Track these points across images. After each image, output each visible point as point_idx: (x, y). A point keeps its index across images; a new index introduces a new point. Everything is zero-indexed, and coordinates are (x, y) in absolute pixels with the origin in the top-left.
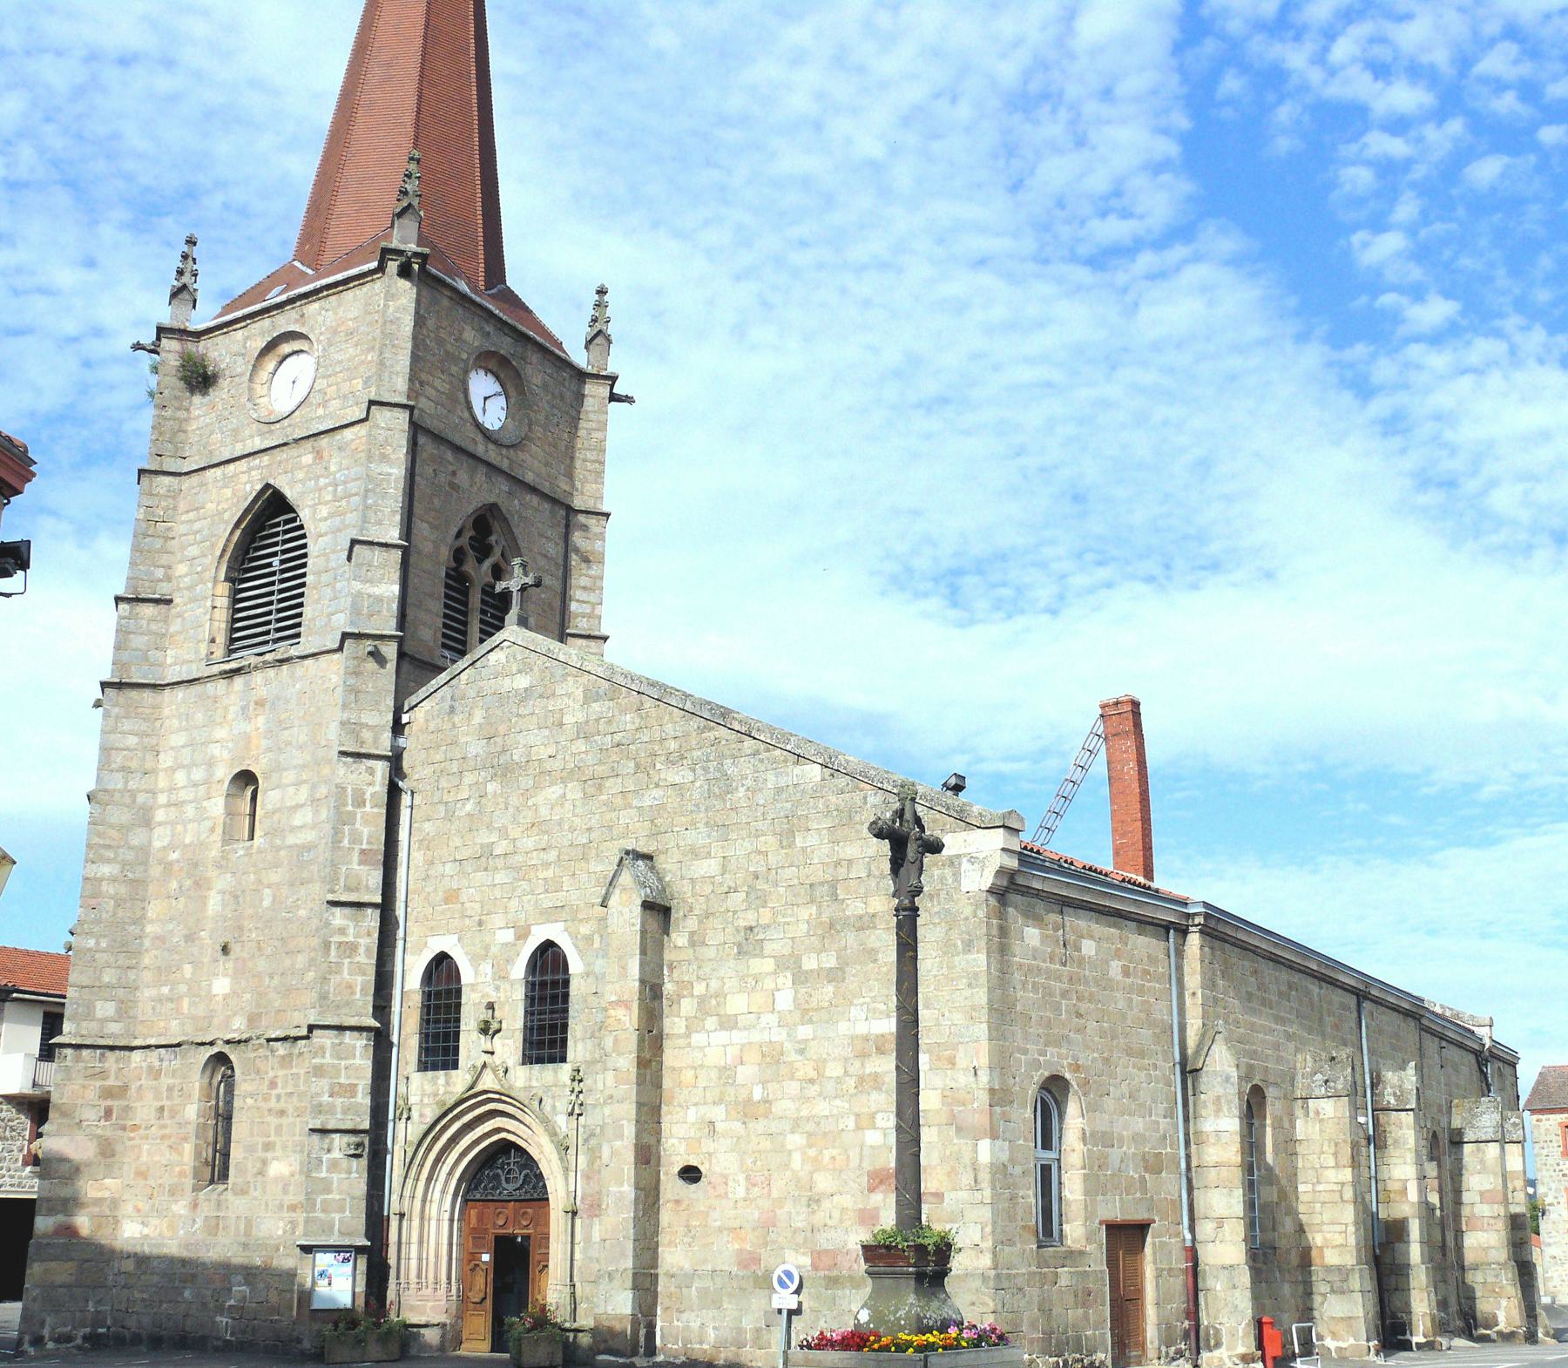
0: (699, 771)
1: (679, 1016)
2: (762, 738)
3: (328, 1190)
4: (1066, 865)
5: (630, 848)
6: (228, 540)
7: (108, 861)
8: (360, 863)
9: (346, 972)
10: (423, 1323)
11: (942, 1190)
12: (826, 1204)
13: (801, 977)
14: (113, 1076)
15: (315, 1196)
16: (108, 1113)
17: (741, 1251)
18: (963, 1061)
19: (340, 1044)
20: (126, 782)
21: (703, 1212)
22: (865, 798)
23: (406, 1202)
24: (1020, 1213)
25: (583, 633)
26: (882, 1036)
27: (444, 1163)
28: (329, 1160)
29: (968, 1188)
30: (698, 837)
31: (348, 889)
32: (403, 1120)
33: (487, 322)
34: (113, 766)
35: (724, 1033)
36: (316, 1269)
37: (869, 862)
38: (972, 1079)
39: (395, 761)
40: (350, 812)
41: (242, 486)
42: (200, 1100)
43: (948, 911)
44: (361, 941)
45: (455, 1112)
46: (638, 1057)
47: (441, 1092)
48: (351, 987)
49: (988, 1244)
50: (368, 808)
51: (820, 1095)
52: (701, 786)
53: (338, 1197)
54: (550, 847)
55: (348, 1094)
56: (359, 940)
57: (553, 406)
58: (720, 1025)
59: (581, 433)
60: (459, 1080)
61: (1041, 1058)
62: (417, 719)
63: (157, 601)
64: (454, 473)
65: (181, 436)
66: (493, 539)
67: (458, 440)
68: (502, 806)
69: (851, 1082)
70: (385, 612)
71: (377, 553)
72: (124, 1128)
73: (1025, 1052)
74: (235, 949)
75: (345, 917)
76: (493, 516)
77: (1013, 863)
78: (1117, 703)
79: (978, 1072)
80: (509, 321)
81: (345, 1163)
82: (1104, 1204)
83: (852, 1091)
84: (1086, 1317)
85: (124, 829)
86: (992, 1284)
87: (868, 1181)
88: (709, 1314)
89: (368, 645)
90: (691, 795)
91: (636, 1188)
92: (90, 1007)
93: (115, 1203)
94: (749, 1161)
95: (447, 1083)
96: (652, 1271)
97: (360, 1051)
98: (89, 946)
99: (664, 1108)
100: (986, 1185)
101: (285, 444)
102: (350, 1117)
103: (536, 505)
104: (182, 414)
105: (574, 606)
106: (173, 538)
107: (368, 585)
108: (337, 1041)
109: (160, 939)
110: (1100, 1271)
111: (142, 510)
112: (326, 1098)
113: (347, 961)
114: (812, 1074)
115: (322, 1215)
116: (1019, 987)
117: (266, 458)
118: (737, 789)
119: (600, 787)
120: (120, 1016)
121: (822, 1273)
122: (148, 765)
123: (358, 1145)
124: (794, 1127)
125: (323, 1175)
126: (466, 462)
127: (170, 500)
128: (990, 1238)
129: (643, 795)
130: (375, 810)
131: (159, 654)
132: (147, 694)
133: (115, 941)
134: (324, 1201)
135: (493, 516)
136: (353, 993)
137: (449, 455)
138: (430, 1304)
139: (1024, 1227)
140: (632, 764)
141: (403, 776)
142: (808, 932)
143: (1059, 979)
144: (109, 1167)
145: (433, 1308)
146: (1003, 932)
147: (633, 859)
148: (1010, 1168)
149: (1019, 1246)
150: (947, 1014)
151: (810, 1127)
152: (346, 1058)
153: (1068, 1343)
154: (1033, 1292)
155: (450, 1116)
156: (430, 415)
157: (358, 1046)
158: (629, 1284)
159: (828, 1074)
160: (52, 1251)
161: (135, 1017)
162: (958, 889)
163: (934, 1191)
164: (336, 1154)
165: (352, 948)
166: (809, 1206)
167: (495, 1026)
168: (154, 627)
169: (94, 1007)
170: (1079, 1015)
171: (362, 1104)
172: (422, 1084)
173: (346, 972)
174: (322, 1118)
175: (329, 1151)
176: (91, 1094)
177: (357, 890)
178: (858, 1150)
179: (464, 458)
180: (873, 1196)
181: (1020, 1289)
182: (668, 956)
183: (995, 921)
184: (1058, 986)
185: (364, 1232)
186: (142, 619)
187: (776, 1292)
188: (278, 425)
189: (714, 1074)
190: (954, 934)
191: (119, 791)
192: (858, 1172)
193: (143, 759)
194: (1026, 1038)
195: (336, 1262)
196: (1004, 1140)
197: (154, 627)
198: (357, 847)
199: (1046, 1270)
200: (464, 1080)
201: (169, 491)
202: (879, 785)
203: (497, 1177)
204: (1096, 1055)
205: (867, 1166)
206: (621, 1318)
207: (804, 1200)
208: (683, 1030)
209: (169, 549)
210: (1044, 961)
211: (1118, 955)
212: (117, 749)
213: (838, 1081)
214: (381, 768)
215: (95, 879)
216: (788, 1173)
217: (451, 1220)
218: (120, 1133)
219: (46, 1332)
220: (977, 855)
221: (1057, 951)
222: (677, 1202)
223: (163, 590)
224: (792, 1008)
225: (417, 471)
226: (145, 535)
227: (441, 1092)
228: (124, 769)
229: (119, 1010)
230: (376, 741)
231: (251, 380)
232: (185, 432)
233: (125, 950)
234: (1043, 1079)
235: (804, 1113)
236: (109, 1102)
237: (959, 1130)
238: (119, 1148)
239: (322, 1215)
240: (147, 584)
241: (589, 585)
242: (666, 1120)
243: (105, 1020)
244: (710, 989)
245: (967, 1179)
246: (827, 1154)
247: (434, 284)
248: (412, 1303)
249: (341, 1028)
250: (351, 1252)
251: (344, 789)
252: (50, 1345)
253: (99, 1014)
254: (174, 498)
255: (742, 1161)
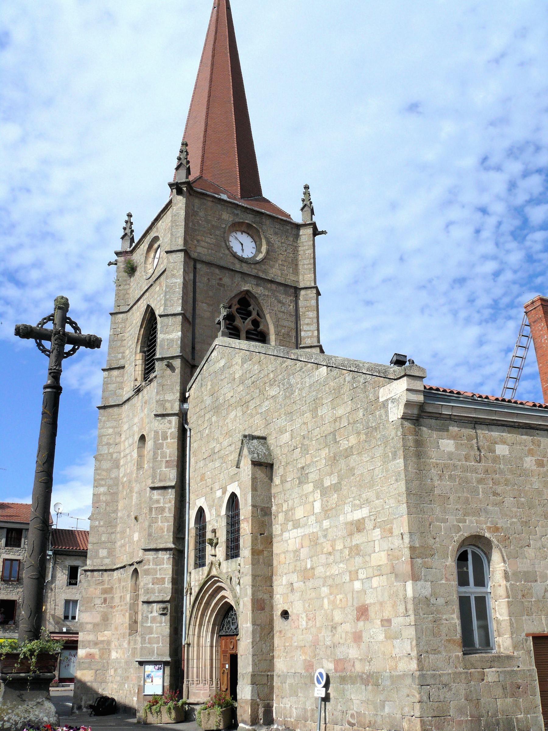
0: (281, 386)
1: (278, 524)
2: (302, 360)
3: (151, 633)
4: (479, 399)
5: (247, 434)
6: (139, 334)
7: (103, 486)
8: (166, 467)
9: (160, 522)
10: (196, 702)
11: (390, 617)
12: (339, 629)
13: (325, 492)
14: (106, 583)
15: (145, 636)
16: (105, 600)
17: (305, 660)
18: (396, 532)
19: (157, 558)
20: (109, 450)
21: (290, 637)
22: (345, 379)
23: (191, 637)
24: (444, 630)
25: (308, 345)
26: (359, 520)
28: (151, 617)
29: (403, 615)
30: (281, 422)
31: (161, 481)
32: (188, 595)
33: (236, 209)
34: (104, 443)
35: (295, 530)
36: (146, 673)
37: (348, 416)
38: (401, 542)
39: (183, 416)
40: (160, 443)
41: (141, 308)
42: (131, 592)
43: (384, 436)
44: (167, 505)
46: (252, 549)
48: (162, 529)
49: (414, 654)
50: (169, 440)
51: (334, 562)
52: (282, 394)
53: (156, 636)
54: (233, 443)
55: (161, 583)
56: (165, 505)
57: (282, 243)
58: (293, 526)
59: (301, 253)
61: (461, 525)
62: (191, 394)
63: (119, 368)
64: (221, 279)
65: (127, 296)
66: (251, 308)
67: (222, 263)
68: (217, 428)
69: (347, 552)
70: (175, 346)
71: (170, 319)
72: (112, 607)
73: (445, 521)
74: (140, 518)
75: (159, 495)
76: (250, 297)
77: (420, 398)
78: (533, 303)
79: (404, 537)
80: (249, 207)
81: (159, 618)
82: (530, 622)
83: (347, 557)
84: (516, 705)
85: (109, 470)
86: (417, 681)
87: (357, 613)
88: (293, 699)
89: (165, 362)
90: (279, 400)
91: (253, 625)
92: (97, 552)
93: (109, 643)
94: (307, 605)
96: (269, 673)
97: (166, 560)
98: (96, 525)
99: (274, 577)
100: (411, 612)
101: (151, 285)
102: (162, 595)
103: (275, 289)
104: (127, 287)
105: (303, 334)
106: (125, 340)
107: (167, 335)
108: (155, 557)
109: (121, 518)
110: (528, 670)
111: (112, 331)
112: (150, 586)
113: (160, 516)
114: (330, 549)
115: (148, 645)
116: (436, 478)
117: (147, 294)
118: (295, 391)
119: (247, 407)
120: (109, 555)
121: (338, 674)
122: (117, 441)
123: (164, 609)
124: (324, 583)
125: (149, 625)
126: (227, 273)
127: (123, 324)
128: (415, 649)
129: (262, 406)
130: (172, 441)
131: (120, 391)
132: (116, 409)
133: (106, 522)
134: (149, 638)
135: (250, 297)
136: (163, 532)
137: (217, 271)
138: (202, 692)
139: (449, 641)
140: (258, 391)
141: (187, 423)
142: (325, 464)
143: (476, 471)
144: (106, 625)
145: (203, 694)
146: (419, 443)
147: (249, 439)
148: (433, 600)
149: (444, 654)
150: (387, 501)
151: (330, 582)
152: (160, 565)
153: (498, 724)
154: (460, 688)
156: (205, 255)
157: (165, 558)
158: (249, 682)
159: (337, 548)
160: (84, 665)
161: (115, 556)
162: (388, 420)
163: (386, 618)
164: (155, 614)
165: (162, 509)
166: (332, 631)
167: (215, 541)
168: (118, 379)
169: (99, 552)
170: (495, 494)
171: (167, 587)
173: (160, 522)
174: (149, 596)
175: (151, 612)
176: (98, 592)
177: (165, 481)
178: (351, 593)
179: (227, 272)
180: (359, 622)
181: (446, 685)
182: (273, 491)
183: (410, 437)
184: (474, 477)
185: (168, 654)
186: (113, 377)
187: (316, 687)
188: (151, 278)
189: (292, 555)
190: (388, 449)
191: (106, 454)
192: (352, 608)
193: (115, 439)
194: (444, 511)
195: (154, 670)
196: (426, 581)
197: (118, 379)
198: (164, 460)
199: (473, 670)
201: (122, 320)
202: (349, 369)
203: (229, 622)
204: (514, 520)
205: (356, 605)
207: (330, 627)
208: (280, 532)
209: (124, 345)
210: (459, 460)
211: (531, 452)
212: (105, 435)
213: (341, 551)
214: (174, 420)
215: (98, 494)
216: (323, 611)
217: (212, 646)
218: (110, 610)
219: (83, 703)
220: (395, 397)
221: (472, 453)
222: (280, 632)
223: (121, 363)
224: (321, 511)
225: (197, 280)
226: (113, 341)
228: (108, 444)
229: (108, 552)
230: (172, 408)
231: (145, 263)
232: (128, 294)
233: (110, 525)
234: (463, 538)
235: (328, 574)
236: (105, 596)
237: (397, 576)
238: (110, 616)
239: (148, 645)
240: (115, 361)
241: (310, 322)
242: (275, 584)
243: (104, 558)
244: (289, 506)
245: (401, 609)
246: (339, 597)
247: (201, 196)
248: (194, 691)
249: (157, 550)
250: (161, 664)
251: (158, 432)
252: (85, 710)
253: (101, 555)
254: (124, 323)
255: (304, 605)
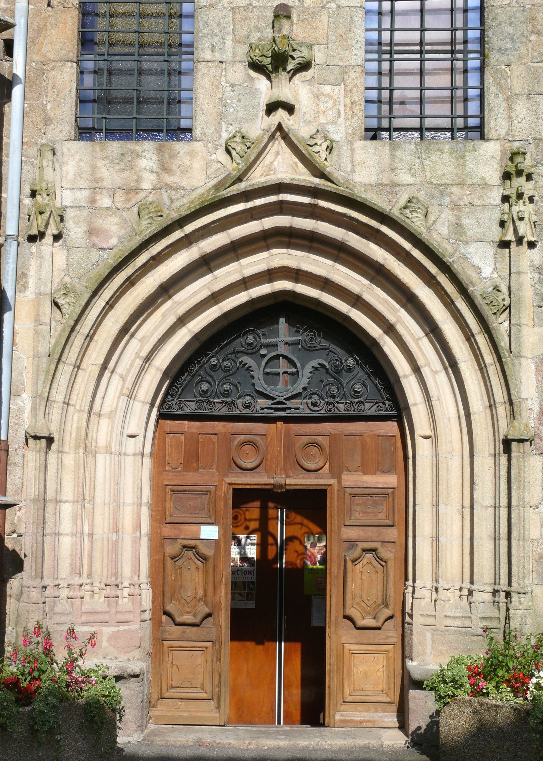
27: (132, 336)
45: (189, 228)
47: (146, 185)
60: (197, 164)
95: (165, 168)
138: (107, 630)
145: (114, 637)
155: (177, 235)
172: (94, 168)
200: (208, 164)
206: (374, 40)
227: (146, 185)
